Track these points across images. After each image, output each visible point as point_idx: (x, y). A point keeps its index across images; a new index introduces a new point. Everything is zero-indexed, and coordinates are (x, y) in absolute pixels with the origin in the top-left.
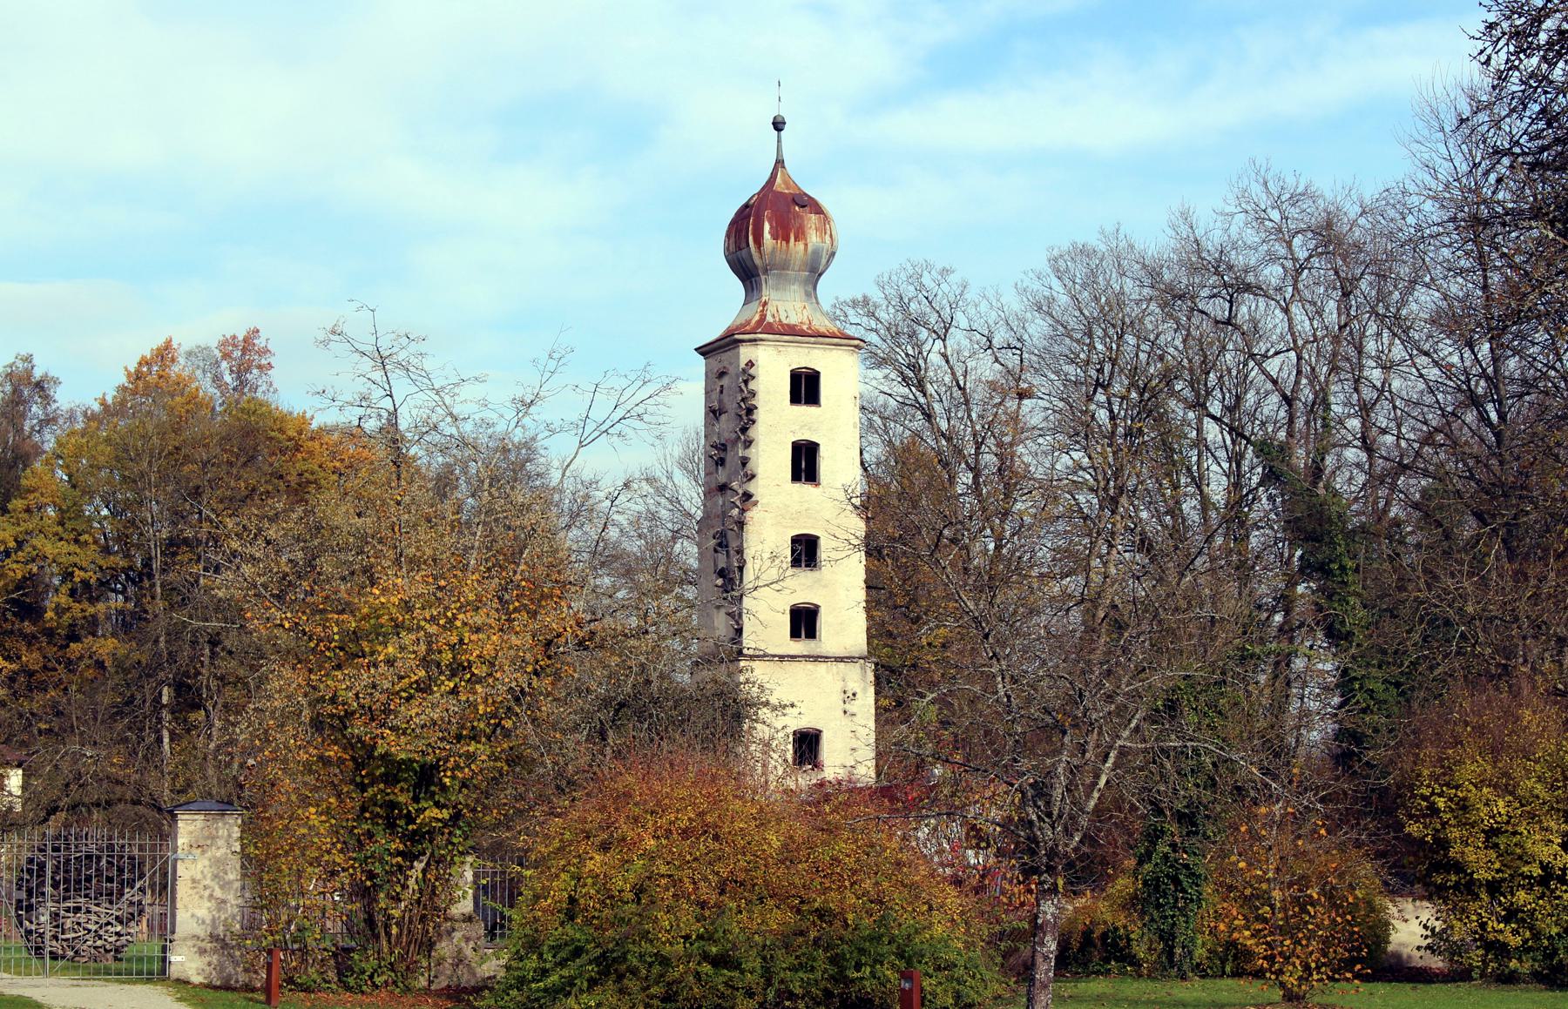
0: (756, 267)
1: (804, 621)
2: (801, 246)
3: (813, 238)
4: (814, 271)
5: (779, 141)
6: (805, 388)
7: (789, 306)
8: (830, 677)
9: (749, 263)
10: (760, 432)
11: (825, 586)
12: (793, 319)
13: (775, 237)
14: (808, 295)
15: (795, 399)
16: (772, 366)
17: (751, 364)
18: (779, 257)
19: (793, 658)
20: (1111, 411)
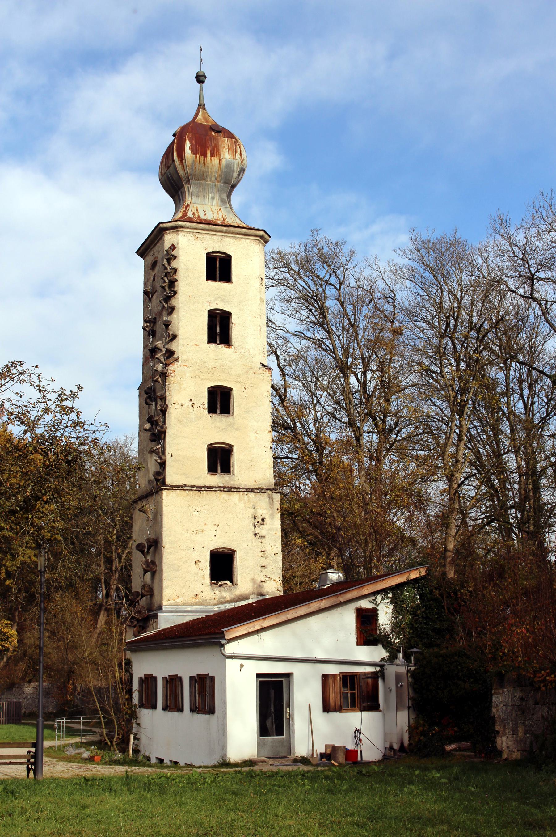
0: (180, 178)
1: (220, 458)
2: (216, 161)
3: (226, 155)
4: (229, 184)
5: (201, 90)
6: (219, 268)
7: (207, 208)
8: (242, 505)
9: (175, 178)
10: (181, 301)
11: (237, 429)
12: (210, 217)
13: (194, 152)
14: (223, 201)
15: (211, 276)
16: (191, 252)
17: (173, 247)
18: (198, 169)
19: (209, 488)
20: (469, 448)
